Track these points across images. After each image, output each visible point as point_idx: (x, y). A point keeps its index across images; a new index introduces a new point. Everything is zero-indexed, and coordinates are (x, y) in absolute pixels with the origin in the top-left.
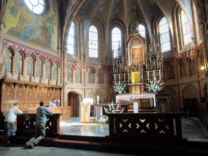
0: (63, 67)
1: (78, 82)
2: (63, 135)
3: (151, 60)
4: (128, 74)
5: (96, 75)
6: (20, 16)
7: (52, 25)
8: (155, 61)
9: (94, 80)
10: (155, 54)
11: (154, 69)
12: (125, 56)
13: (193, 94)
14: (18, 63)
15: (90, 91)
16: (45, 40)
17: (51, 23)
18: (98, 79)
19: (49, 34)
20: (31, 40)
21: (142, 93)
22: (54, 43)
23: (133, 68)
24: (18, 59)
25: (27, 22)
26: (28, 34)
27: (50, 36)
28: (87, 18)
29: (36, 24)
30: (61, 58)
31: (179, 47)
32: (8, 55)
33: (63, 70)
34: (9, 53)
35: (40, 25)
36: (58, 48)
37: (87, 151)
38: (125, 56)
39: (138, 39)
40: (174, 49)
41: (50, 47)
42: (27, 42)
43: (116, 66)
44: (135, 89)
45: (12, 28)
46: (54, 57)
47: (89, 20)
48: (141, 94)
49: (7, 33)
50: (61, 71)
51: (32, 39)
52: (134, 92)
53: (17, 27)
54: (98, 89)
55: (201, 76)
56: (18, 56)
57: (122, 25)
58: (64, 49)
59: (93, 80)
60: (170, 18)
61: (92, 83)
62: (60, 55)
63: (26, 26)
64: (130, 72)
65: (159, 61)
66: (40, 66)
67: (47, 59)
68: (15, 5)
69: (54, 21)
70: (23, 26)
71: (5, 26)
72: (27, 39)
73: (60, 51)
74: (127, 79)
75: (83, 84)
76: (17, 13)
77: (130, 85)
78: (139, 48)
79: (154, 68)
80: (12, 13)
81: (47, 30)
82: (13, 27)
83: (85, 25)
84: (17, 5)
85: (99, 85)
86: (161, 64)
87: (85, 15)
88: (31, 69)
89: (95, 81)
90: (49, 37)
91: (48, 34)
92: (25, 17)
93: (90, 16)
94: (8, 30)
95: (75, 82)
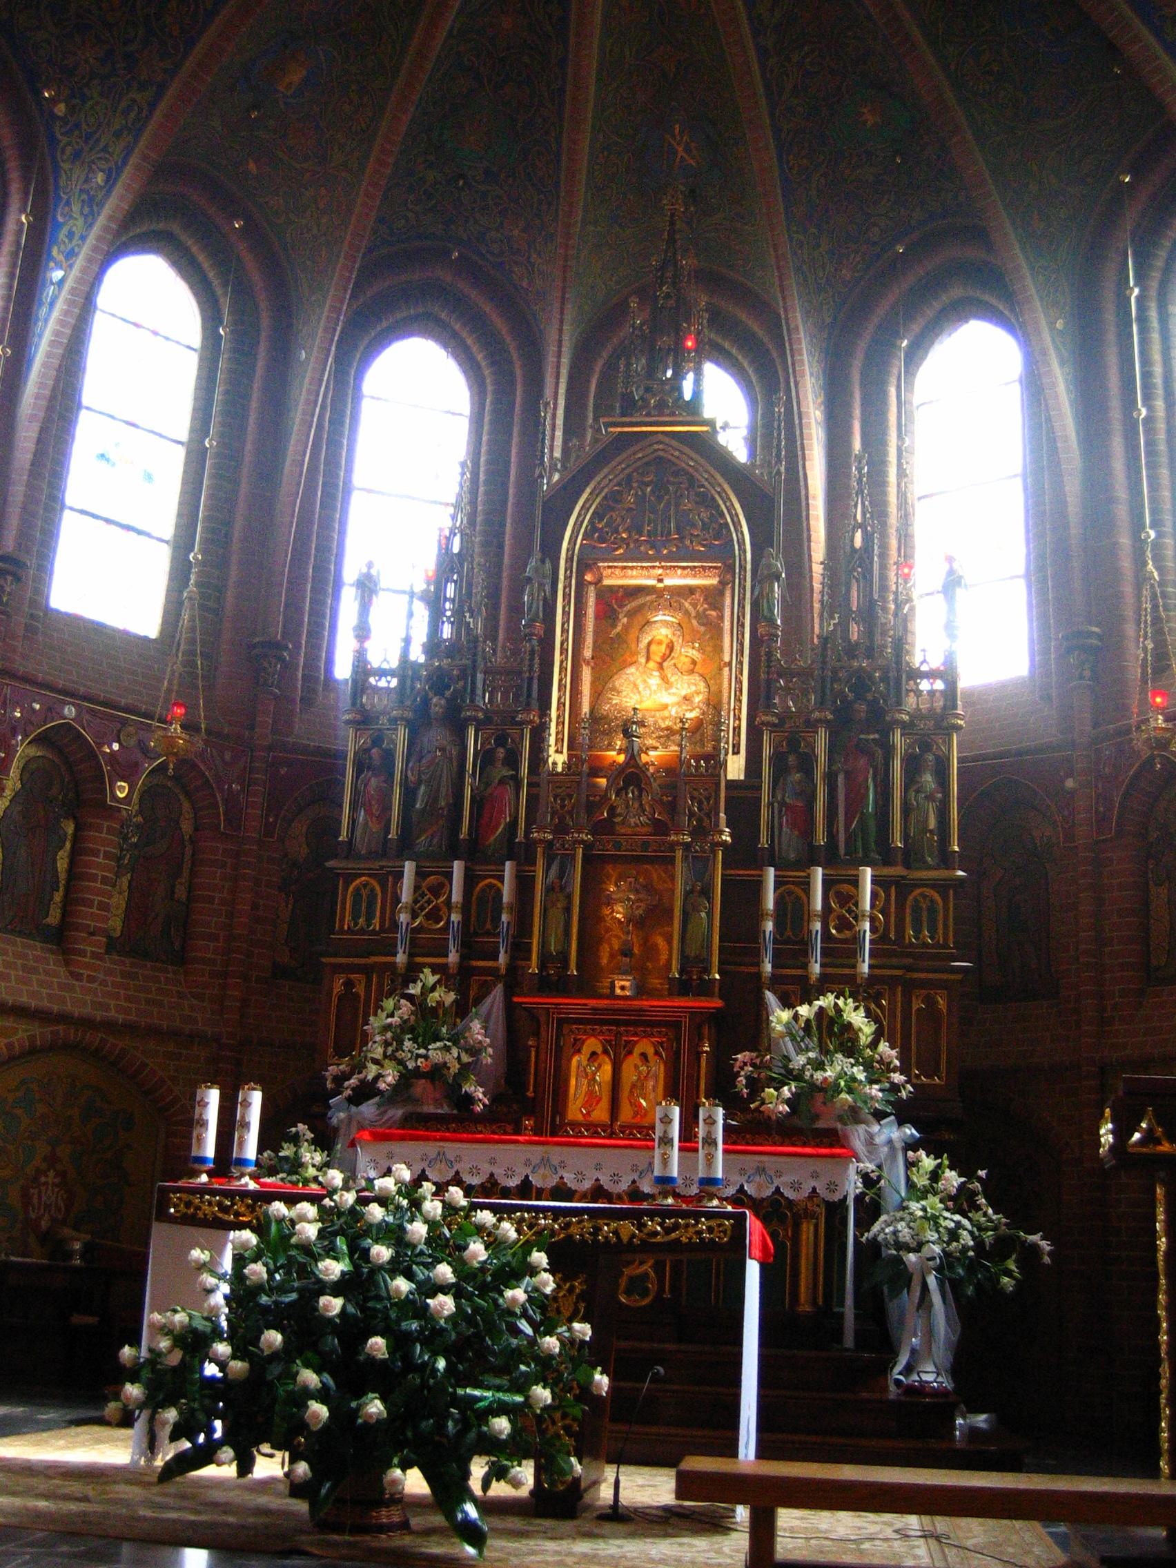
2: (191, 1145)
8: (871, 756)
18: (118, 901)
23: (612, 810)
28: (118, 135)
31: (715, 922)
37: (985, 1473)
39: (692, 481)
47: (128, 152)
54: (109, 1026)
59: (58, 897)
60: (1059, 324)
83: (76, 208)
93: (152, 106)
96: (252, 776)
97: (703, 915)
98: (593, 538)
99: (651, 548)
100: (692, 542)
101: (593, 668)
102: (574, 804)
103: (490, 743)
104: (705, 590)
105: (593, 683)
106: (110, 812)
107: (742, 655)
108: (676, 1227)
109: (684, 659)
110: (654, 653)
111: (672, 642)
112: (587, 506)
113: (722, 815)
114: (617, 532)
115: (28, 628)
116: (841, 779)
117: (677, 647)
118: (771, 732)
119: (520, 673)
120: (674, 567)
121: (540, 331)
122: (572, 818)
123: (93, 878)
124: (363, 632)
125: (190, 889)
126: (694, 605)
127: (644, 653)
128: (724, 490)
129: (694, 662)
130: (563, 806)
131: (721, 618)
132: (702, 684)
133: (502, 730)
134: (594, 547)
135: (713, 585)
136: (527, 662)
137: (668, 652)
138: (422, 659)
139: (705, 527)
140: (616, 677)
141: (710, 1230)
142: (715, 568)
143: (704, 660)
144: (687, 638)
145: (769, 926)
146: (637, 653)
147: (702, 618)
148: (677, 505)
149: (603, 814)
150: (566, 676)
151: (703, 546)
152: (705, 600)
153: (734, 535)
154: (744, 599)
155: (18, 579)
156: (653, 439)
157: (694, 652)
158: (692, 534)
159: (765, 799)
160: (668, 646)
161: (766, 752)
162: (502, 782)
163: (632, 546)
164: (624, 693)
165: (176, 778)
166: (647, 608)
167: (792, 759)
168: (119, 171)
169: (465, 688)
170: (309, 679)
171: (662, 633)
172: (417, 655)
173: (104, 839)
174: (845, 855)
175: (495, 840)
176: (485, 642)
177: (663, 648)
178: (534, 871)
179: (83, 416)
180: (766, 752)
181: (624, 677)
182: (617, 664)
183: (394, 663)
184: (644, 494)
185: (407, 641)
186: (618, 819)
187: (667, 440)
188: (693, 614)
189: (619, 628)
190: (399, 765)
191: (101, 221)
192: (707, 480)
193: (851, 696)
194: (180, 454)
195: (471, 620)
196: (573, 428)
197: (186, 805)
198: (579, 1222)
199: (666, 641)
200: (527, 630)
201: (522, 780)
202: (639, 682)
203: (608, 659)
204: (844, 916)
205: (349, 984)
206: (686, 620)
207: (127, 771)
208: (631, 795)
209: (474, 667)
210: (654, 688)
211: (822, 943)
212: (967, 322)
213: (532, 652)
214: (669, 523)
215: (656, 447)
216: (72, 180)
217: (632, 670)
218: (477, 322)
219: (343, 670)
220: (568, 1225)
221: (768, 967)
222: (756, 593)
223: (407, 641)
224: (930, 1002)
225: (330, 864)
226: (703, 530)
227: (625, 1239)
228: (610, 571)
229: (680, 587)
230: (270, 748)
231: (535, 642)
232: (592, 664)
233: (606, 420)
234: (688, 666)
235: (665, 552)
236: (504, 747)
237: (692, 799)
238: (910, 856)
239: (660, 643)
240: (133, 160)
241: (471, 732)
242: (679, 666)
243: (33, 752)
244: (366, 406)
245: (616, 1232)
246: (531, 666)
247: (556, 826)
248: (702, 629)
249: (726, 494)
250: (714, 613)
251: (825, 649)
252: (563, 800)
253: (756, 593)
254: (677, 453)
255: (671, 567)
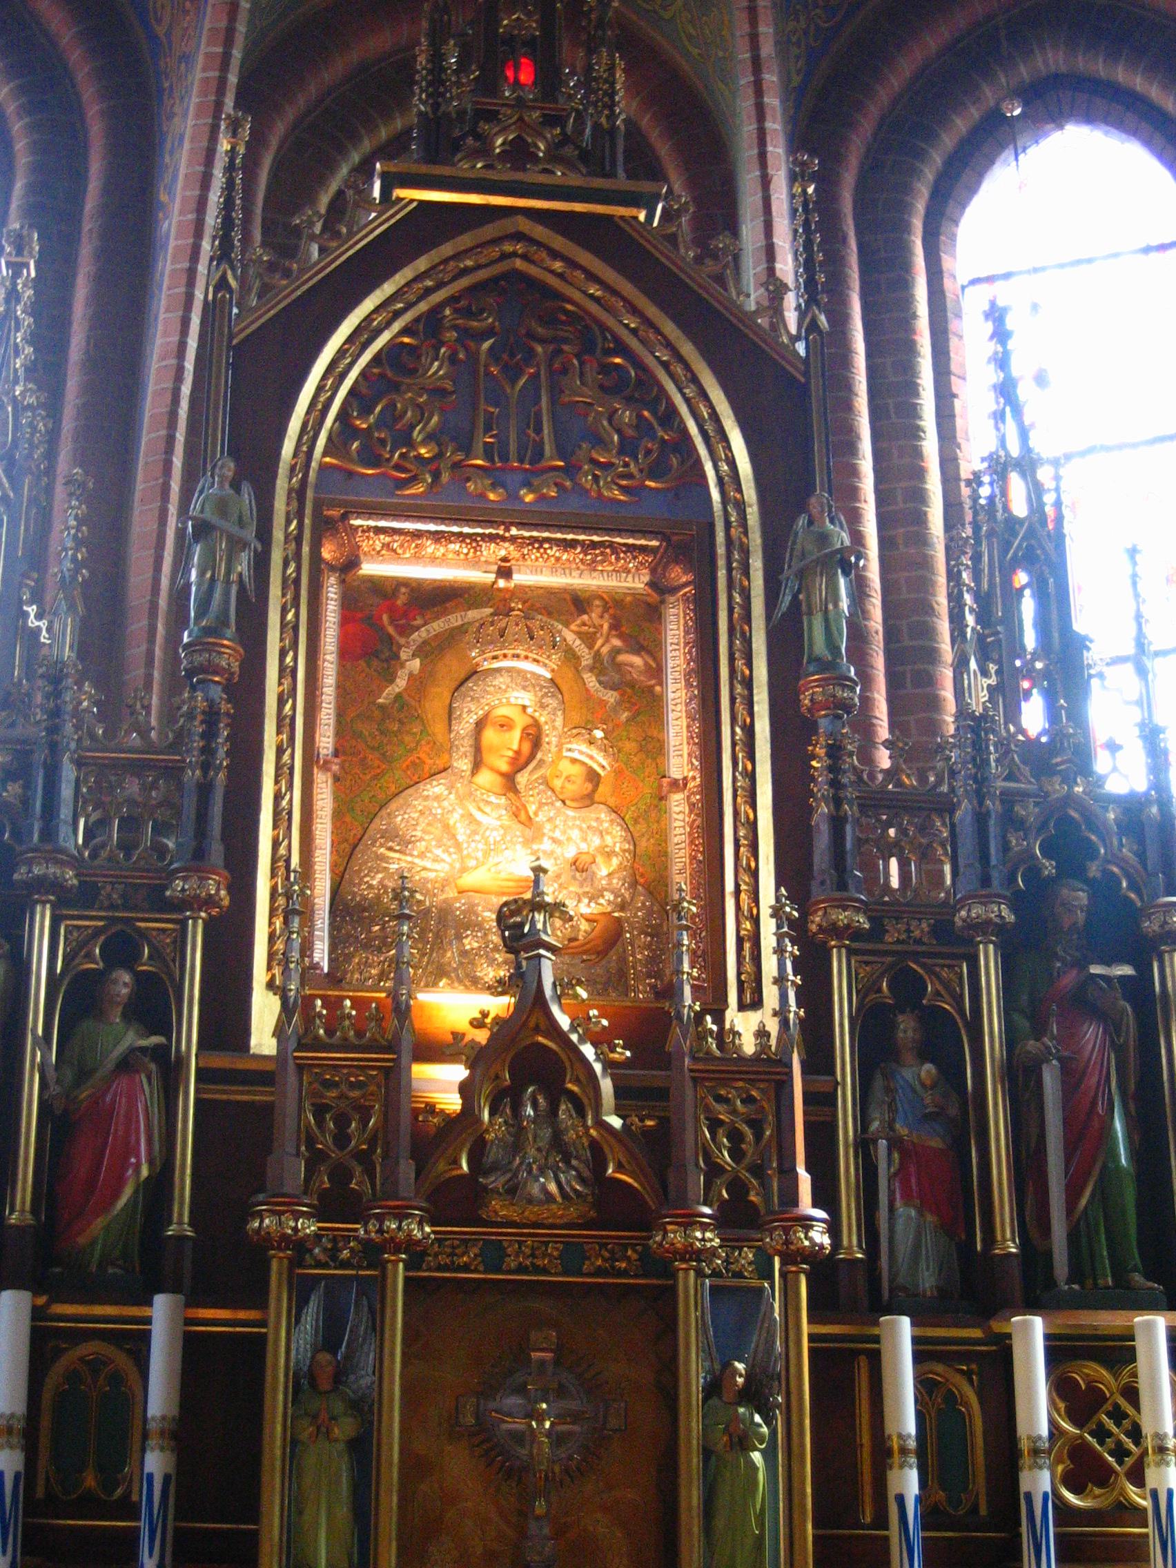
96: (863, 1358)
97: (756, 1457)
98: (348, 452)
99: (494, 486)
100: (596, 478)
101: (336, 779)
102: (376, 1131)
103: (89, 956)
104: (614, 605)
105: (338, 815)
107: (751, 756)
109: (566, 767)
110: (491, 749)
111: (536, 724)
112: (341, 367)
113: (801, 1171)
114: (411, 444)
116: (1050, 1078)
117: (551, 738)
118: (851, 952)
119: (173, 772)
120: (542, 541)
121: (153, 37)
122: (370, 1172)
126: (588, 639)
127: (466, 746)
128: (681, 359)
129: (593, 777)
130: (342, 1139)
131: (657, 672)
132: (618, 831)
133: (127, 921)
134: (351, 474)
135: (635, 594)
136: (198, 743)
137: (526, 748)
139: (627, 448)
140: (393, 805)
142: (643, 549)
143: (618, 773)
144: (576, 717)
145: (909, 1482)
146: (450, 748)
148: (556, 392)
149: (456, 1162)
150: (290, 787)
151: (624, 489)
152: (612, 627)
153: (708, 468)
154: (747, 617)
156: (508, 225)
157: (594, 752)
158: (594, 462)
160: (525, 733)
162: (126, 1065)
163: (445, 477)
164: (421, 846)
166: (470, 637)
167: (906, 1028)
169: (26, 802)
174: (1070, 1281)
175: (107, 1228)
176: (80, 684)
177: (514, 739)
178: (263, 1323)
181: (419, 804)
182: (398, 774)
184: (473, 356)
186: (495, 1181)
187: (539, 231)
188: (587, 660)
189: (401, 683)
192: (634, 332)
193: (1049, 867)
195: (32, 622)
199: (520, 721)
200: (199, 659)
201: (182, 1062)
202: (454, 819)
203: (372, 758)
204: (1085, 1446)
206: (570, 674)
208: (530, 1111)
209: (54, 748)
210: (495, 835)
211: (1055, 1526)
212: (1061, 127)
213: (211, 717)
214: (539, 430)
215: (508, 248)
217: (436, 788)
222: (786, 601)
226: (622, 451)
228: (385, 539)
229: (550, 592)
231: (217, 693)
232: (335, 768)
233: (393, 167)
234: (579, 786)
235: (529, 498)
236: (130, 967)
237: (715, 1124)
239: (506, 725)
241: (43, 919)
242: (557, 783)
246: (208, 751)
247: (323, 1195)
248: (611, 697)
249: (687, 367)
250: (637, 660)
251: (979, 747)
252: (342, 1121)
253: (786, 601)
254: (558, 265)
255: (535, 540)
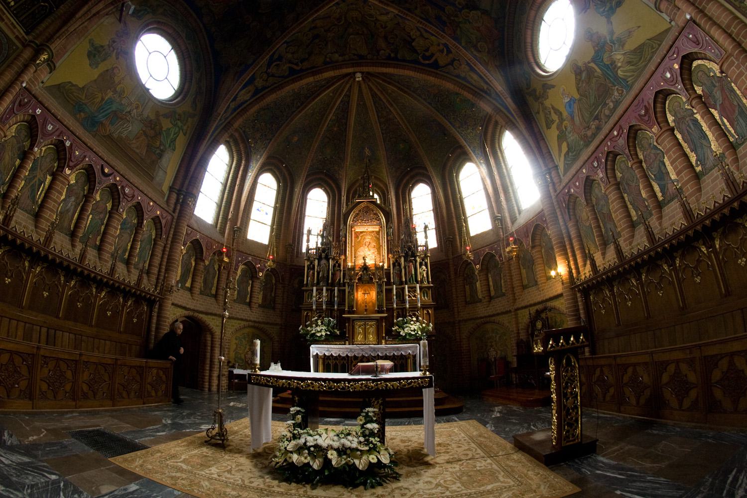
0: (172, 242)
1: (208, 295)
3: (403, 259)
4: (345, 290)
5: (257, 285)
6: (107, 70)
7: (176, 131)
9: (251, 297)
10: (414, 247)
11: (410, 281)
12: (339, 244)
13: (495, 341)
14: (36, 179)
15: (239, 324)
16: (144, 154)
17: (175, 125)
18: (260, 297)
19: (160, 145)
20: (104, 136)
21: (383, 341)
22: (166, 172)
24: (43, 168)
25: (115, 91)
26: (103, 117)
27: (163, 151)
29: (137, 108)
30: (174, 214)
32: (18, 142)
33: (170, 249)
34: (26, 139)
35: (145, 115)
36: (171, 189)
38: (339, 244)
40: (323, 253)
41: (152, 178)
42: (93, 136)
43: (314, 266)
44: (365, 330)
45: (70, 82)
46: (151, 204)
48: (379, 343)
49: (50, 89)
50: (164, 251)
51: (108, 133)
52: (360, 338)
53: (83, 88)
54: (259, 322)
55: (519, 299)
56: (48, 160)
57: (333, 185)
58: (186, 193)
59: (249, 296)
61: (245, 303)
62: (173, 206)
63: (109, 98)
64: (351, 286)
65: (421, 264)
66: (102, 216)
67: (129, 199)
68: (109, 45)
69: (184, 125)
70: (100, 94)
71: (51, 65)
72: (95, 129)
73: (174, 196)
74: (342, 302)
75: (222, 303)
76: (102, 61)
77: (349, 318)
78: (373, 232)
79: (410, 279)
80: (90, 55)
81: (160, 134)
82: (74, 83)
84: (113, 48)
85: (263, 312)
86: (427, 271)
87: (259, 142)
88: (70, 214)
89: (254, 300)
90: (158, 151)
91: (158, 143)
92: (117, 80)
93: (269, 143)
94: (57, 83)
95: (201, 294)
104: (376, 231)
106: (258, 279)
108: (411, 382)
115: (243, 242)
123: (255, 292)
124: (308, 241)
125: (275, 294)
138: (320, 246)
141: (422, 382)
145: (395, 297)
147: (376, 237)
155: (240, 232)
159: (392, 272)
161: (391, 262)
165: (270, 271)
167: (396, 264)
168: (262, 154)
170: (298, 252)
171: (367, 240)
172: (319, 245)
173: (257, 285)
179: (255, 202)
180: (391, 262)
183: (315, 247)
185: (317, 242)
190: (316, 268)
191: (259, 163)
194: (272, 209)
196: (347, 205)
197: (273, 278)
198: (381, 383)
205: (307, 313)
207: (261, 270)
216: (254, 157)
218: (329, 185)
219: (304, 250)
220: (377, 385)
221: (395, 306)
223: (317, 242)
224: (428, 311)
225: (303, 288)
227: (396, 387)
230: (290, 266)
238: (422, 282)
240: (265, 152)
243: (243, 267)
244: (308, 201)
245: (392, 386)
